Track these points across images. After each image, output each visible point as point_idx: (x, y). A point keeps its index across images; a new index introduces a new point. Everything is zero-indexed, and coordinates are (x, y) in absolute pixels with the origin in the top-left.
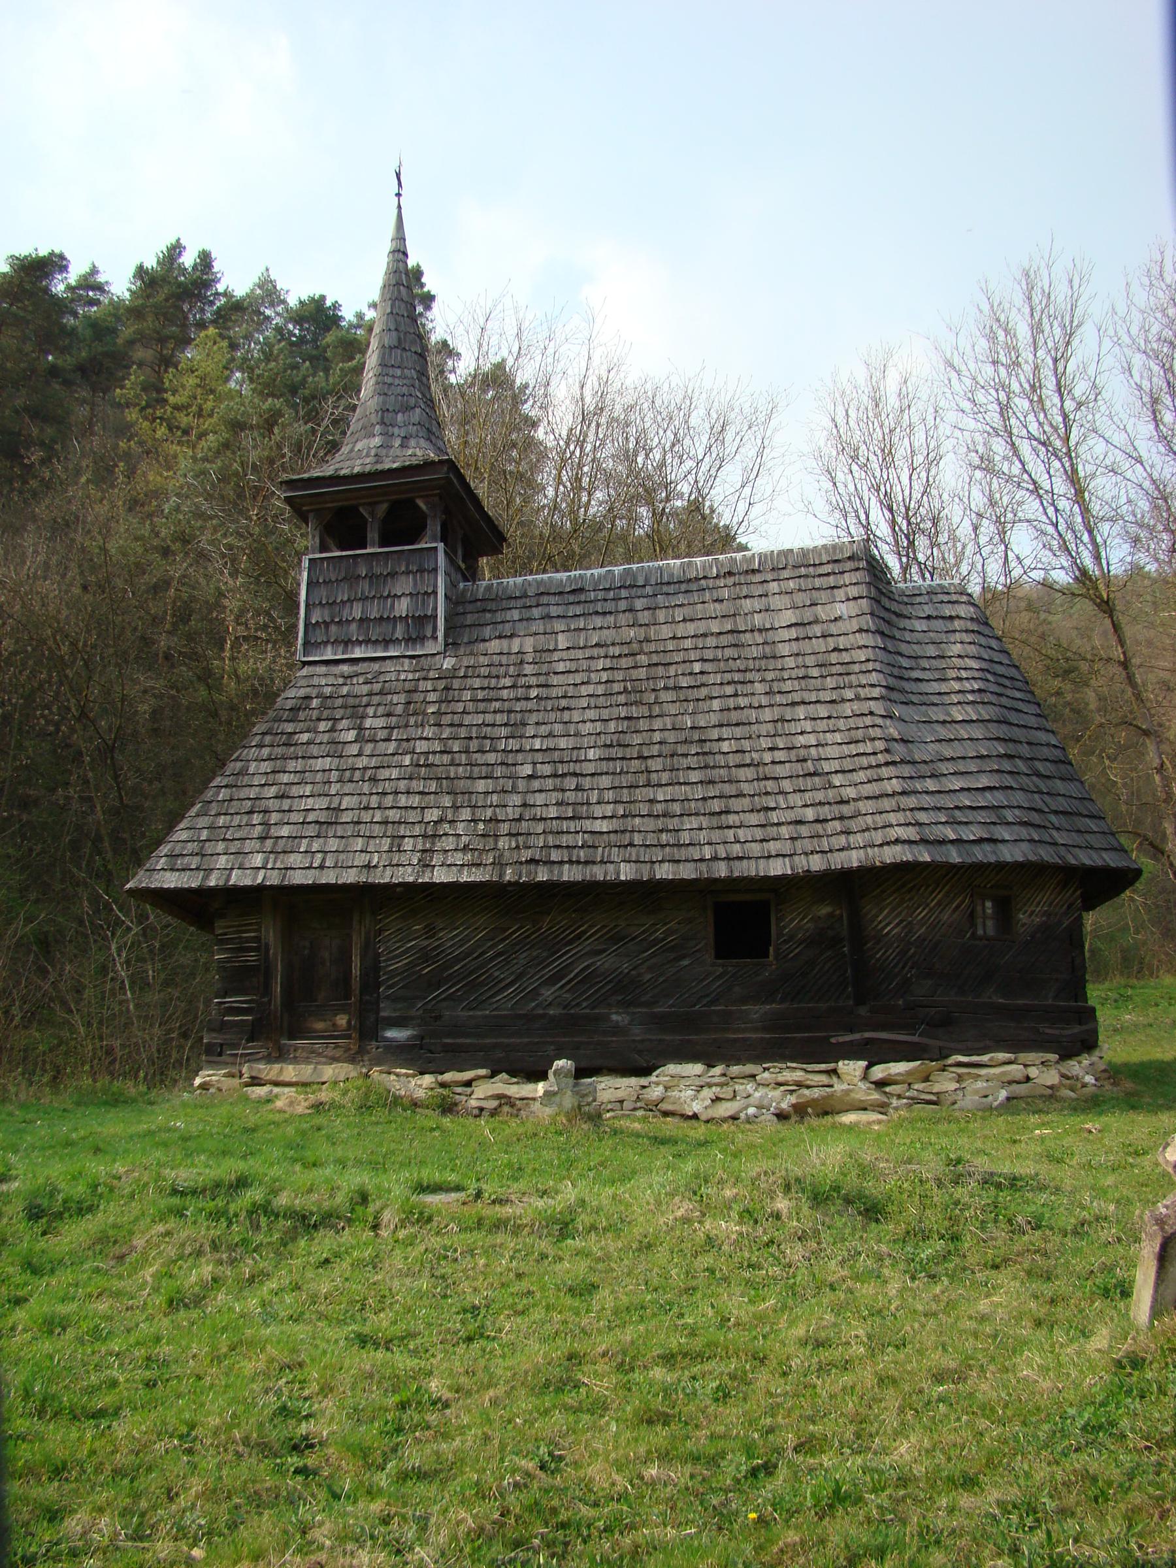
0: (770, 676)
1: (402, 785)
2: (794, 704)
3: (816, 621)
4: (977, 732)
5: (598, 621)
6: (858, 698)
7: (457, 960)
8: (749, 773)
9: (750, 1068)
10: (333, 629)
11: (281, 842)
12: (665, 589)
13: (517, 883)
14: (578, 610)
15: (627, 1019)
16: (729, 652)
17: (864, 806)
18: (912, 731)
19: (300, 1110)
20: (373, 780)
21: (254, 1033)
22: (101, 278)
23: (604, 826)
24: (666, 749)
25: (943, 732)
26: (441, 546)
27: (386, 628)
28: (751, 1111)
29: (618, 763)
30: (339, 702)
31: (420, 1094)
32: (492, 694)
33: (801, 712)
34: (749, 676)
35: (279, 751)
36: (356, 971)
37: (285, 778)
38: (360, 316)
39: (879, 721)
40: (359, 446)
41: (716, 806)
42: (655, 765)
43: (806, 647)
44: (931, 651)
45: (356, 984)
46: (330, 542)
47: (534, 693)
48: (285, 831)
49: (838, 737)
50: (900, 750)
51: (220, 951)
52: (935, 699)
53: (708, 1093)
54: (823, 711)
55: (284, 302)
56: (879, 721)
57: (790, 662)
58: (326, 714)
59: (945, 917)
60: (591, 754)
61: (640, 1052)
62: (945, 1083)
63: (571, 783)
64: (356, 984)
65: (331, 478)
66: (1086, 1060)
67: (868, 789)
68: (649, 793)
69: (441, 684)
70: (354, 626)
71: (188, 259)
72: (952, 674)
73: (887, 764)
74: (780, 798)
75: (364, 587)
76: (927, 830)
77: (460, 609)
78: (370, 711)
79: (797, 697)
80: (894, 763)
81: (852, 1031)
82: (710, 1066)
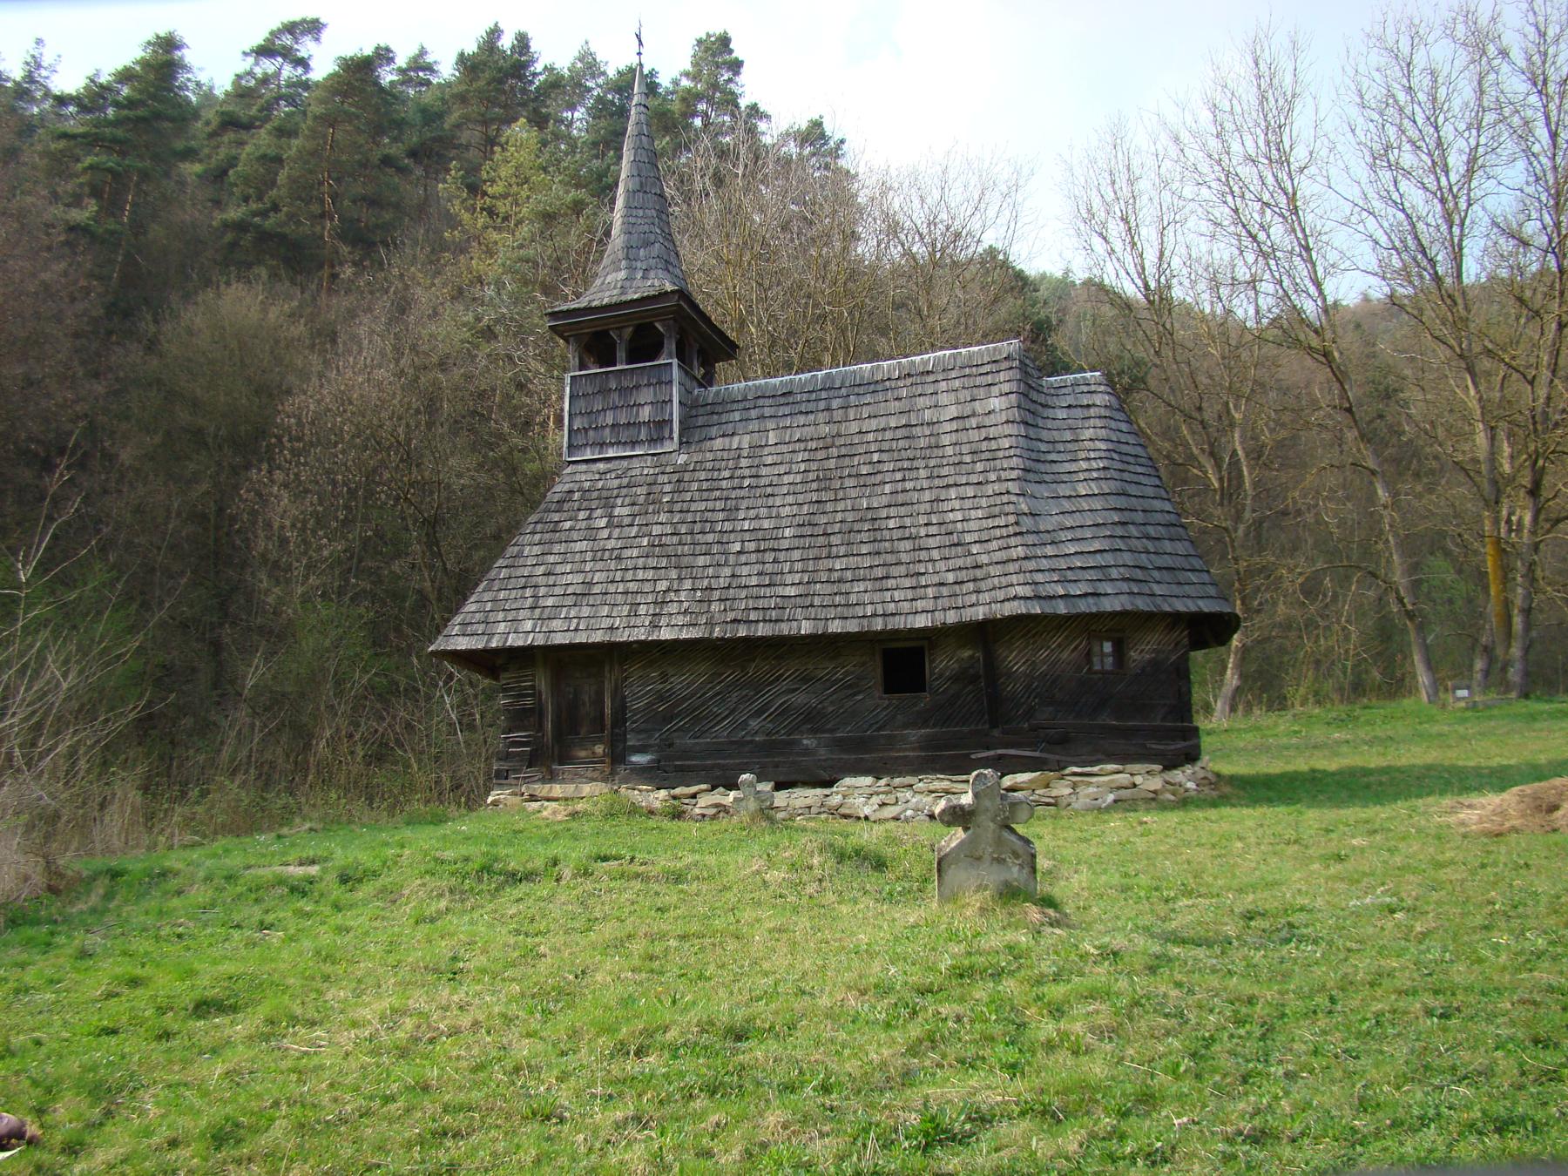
0: (932, 463)
1: (641, 562)
2: (948, 486)
3: (974, 415)
4: (1097, 504)
5: (802, 419)
6: (999, 480)
7: (685, 699)
8: (908, 545)
9: (909, 780)
10: (591, 433)
11: (547, 611)
12: (856, 390)
13: (723, 639)
14: (787, 410)
15: (815, 743)
16: (902, 444)
17: (993, 570)
18: (1040, 506)
19: (559, 817)
20: (619, 558)
21: (533, 760)
22: (429, 59)
23: (792, 591)
24: (846, 527)
25: (1067, 505)
26: (675, 361)
27: (633, 431)
28: (909, 813)
29: (808, 540)
30: (595, 495)
31: (657, 804)
32: (715, 484)
33: (953, 493)
34: (916, 464)
35: (547, 536)
36: (608, 711)
37: (551, 559)
38: (676, 83)
39: (1014, 499)
40: (609, 279)
41: (879, 572)
42: (835, 540)
43: (963, 437)
44: (1068, 436)
45: (608, 722)
46: (590, 361)
47: (746, 483)
48: (550, 602)
49: (980, 513)
50: (1027, 523)
51: (505, 697)
52: (1065, 478)
53: (875, 800)
54: (970, 491)
55: (604, 73)
56: (1014, 499)
57: (949, 451)
58: (585, 504)
59: (1065, 655)
60: (787, 532)
61: (825, 769)
62: (1062, 789)
63: (769, 556)
64: (608, 722)
65: (585, 309)
66: (1189, 769)
67: (998, 556)
68: (829, 563)
69: (675, 477)
70: (607, 430)
71: (506, 42)
72: (1083, 455)
73: (1016, 534)
74: (930, 565)
75: (615, 398)
76: (1041, 588)
77: (694, 412)
78: (619, 501)
79: (951, 481)
80: (1021, 533)
81: (988, 749)
82: (879, 778)
